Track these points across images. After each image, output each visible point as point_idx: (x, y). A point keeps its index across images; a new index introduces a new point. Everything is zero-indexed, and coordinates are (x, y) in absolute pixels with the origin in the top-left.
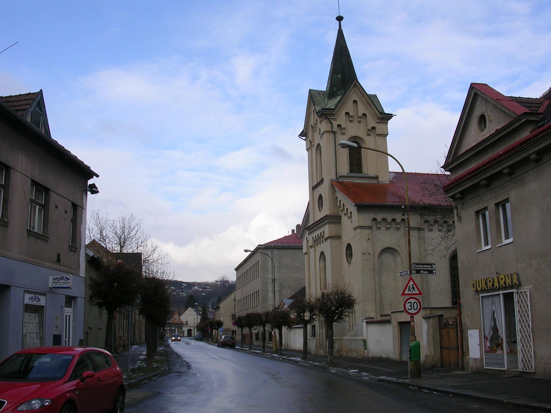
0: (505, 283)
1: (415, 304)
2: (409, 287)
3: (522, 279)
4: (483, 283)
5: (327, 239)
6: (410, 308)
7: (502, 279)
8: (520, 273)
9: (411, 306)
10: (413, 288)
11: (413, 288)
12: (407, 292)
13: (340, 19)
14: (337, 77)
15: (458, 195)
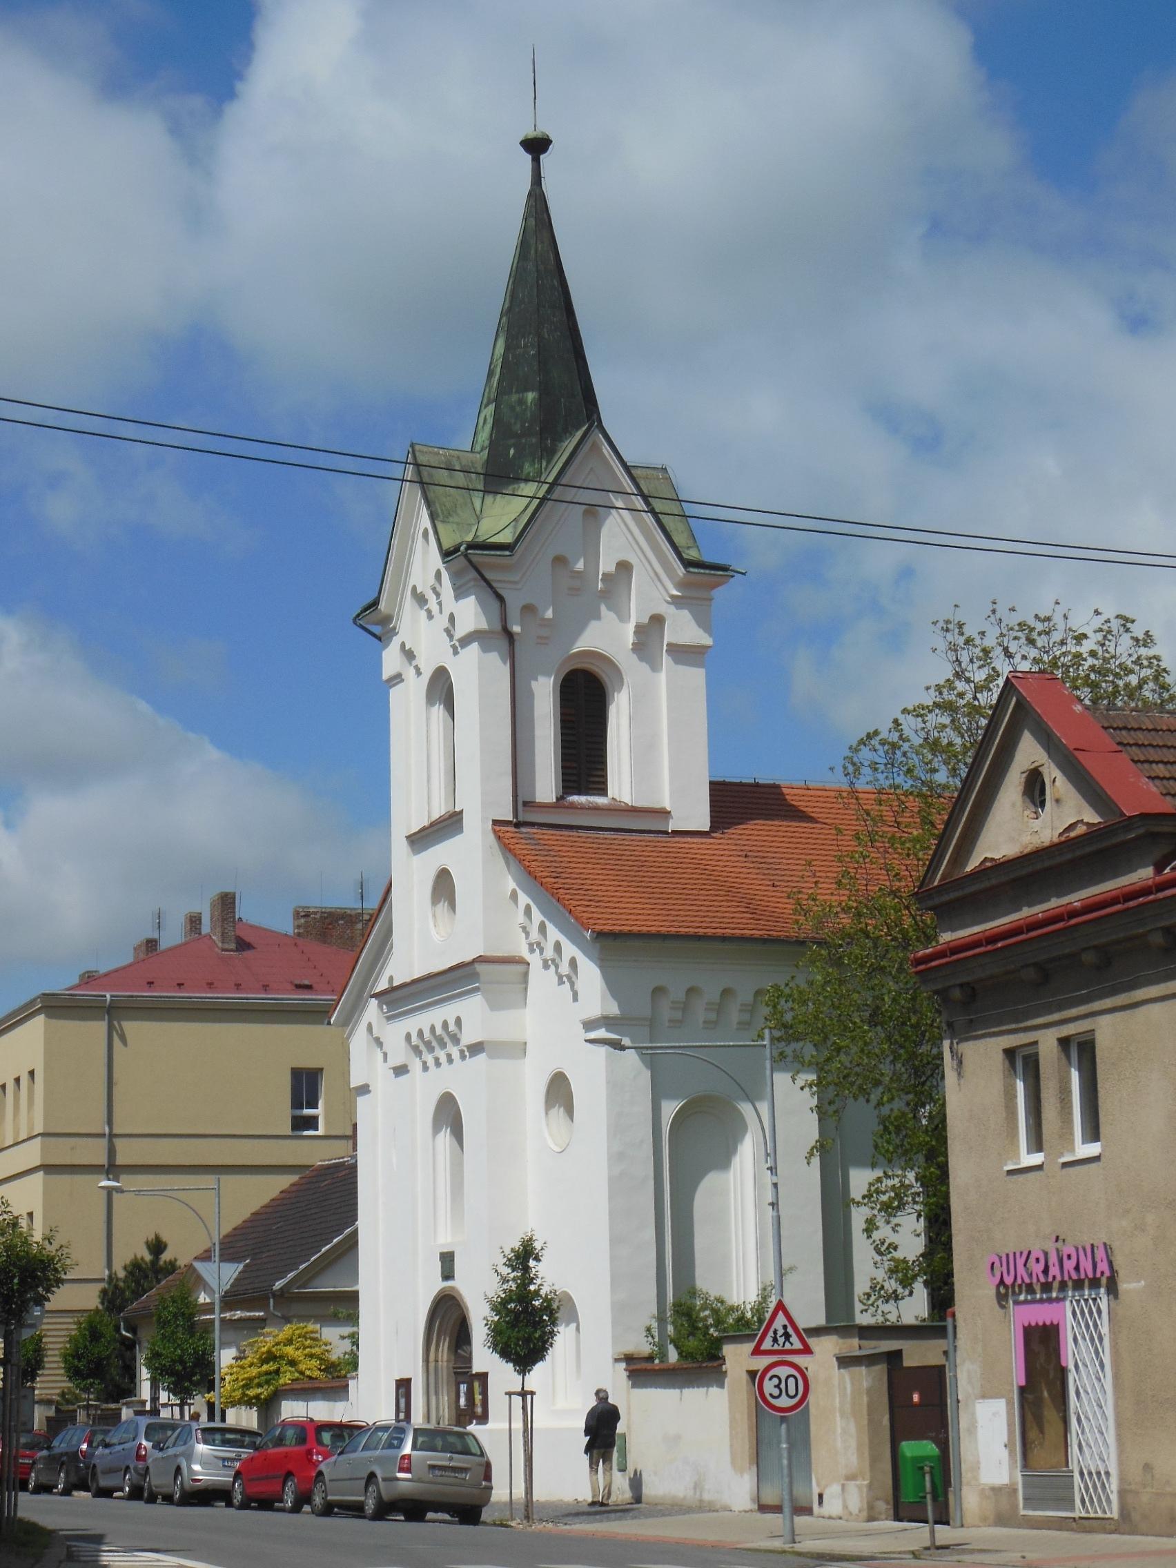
0: (1077, 1268)
1: (791, 1380)
2: (775, 1332)
3: (1119, 1261)
4: (1020, 1262)
6: (776, 1392)
7: (1069, 1257)
8: (1116, 1245)
9: (778, 1386)
10: (787, 1336)
11: (787, 1336)
12: (781, 1320)
13: (536, 146)
14: (521, 402)
15: (957, 994)
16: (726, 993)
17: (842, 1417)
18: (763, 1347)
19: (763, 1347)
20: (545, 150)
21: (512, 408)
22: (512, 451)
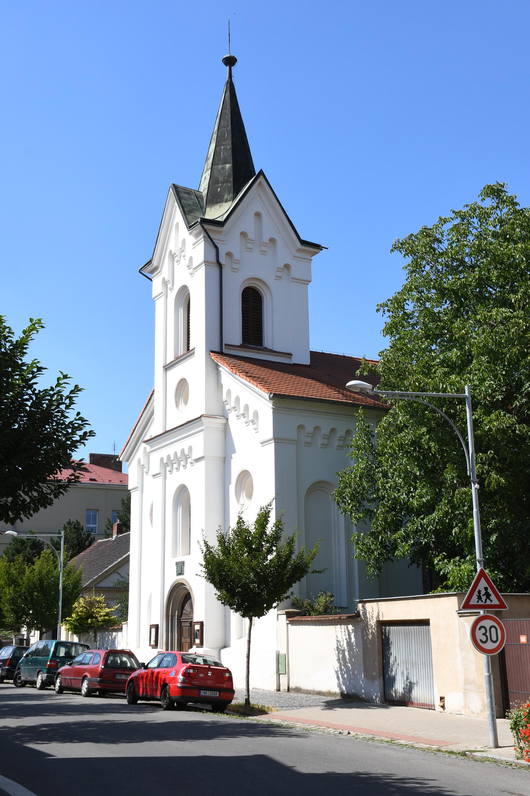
1: (493, 630)
2: (479, 592)
5: (197, 460)
6: (484, 639)
9: (485, 634)
10: (488, 595)
11: (488, 595)
13: (230, 61)
14: (223, 168)
16: (333, 430)
17: (461, 650)
18: (471, 603)
19: (471, 603)
20: (233, 65)
21: (219, 171)
22: (219, 189)
